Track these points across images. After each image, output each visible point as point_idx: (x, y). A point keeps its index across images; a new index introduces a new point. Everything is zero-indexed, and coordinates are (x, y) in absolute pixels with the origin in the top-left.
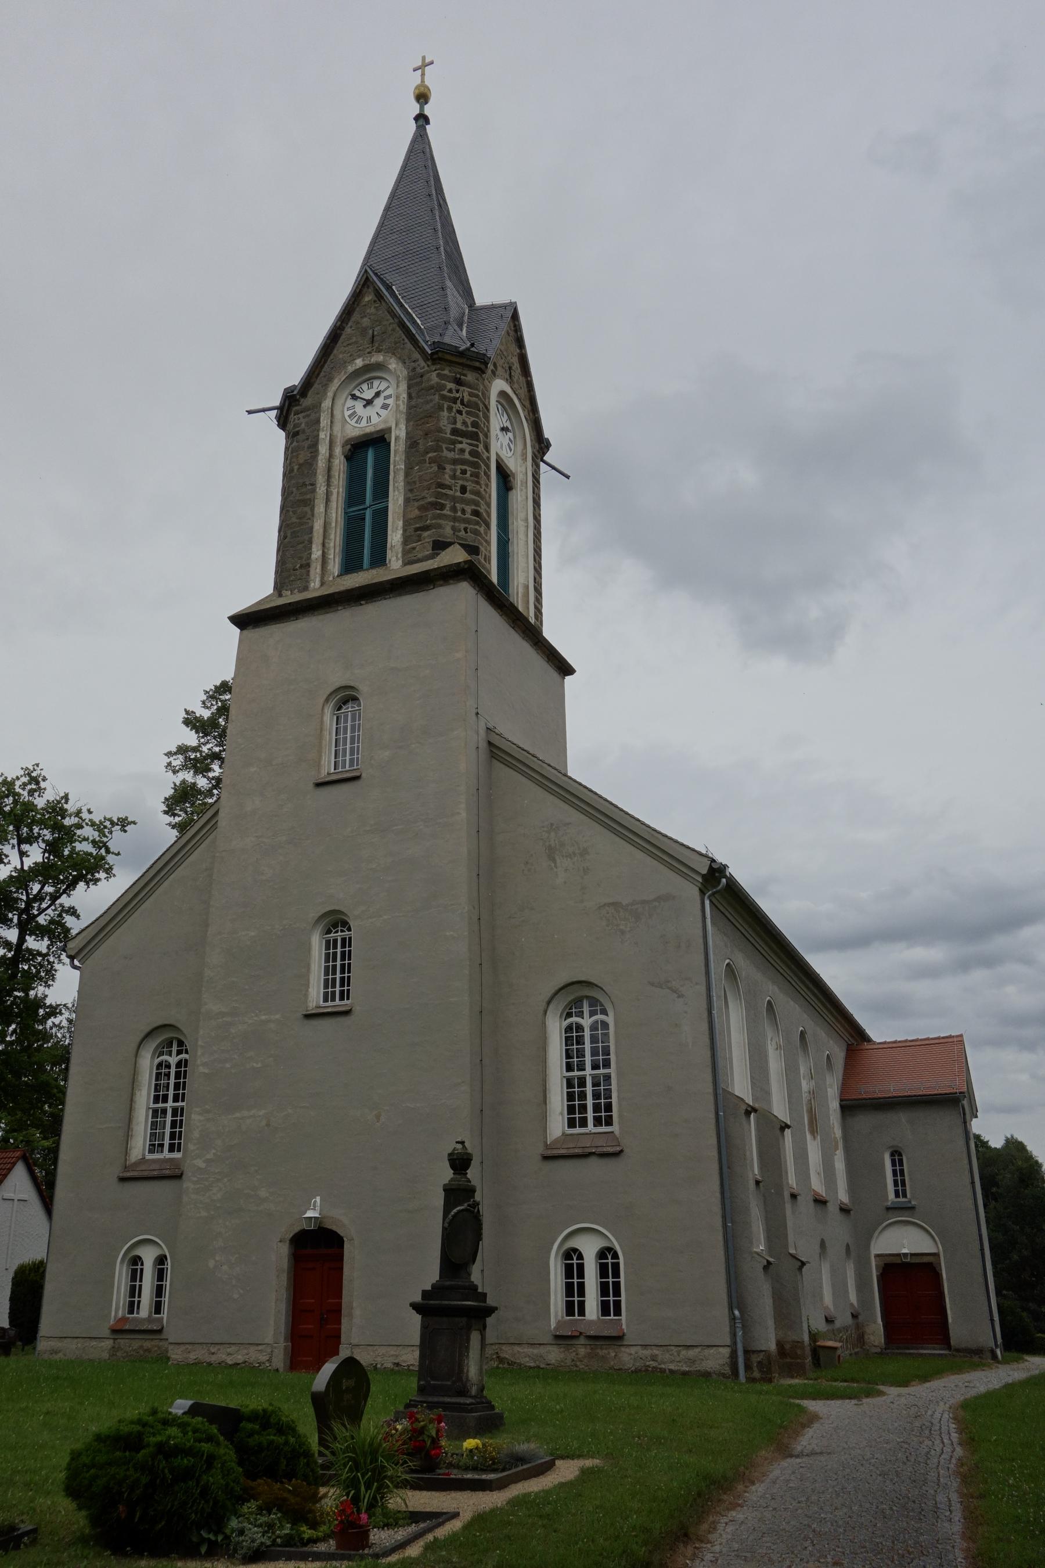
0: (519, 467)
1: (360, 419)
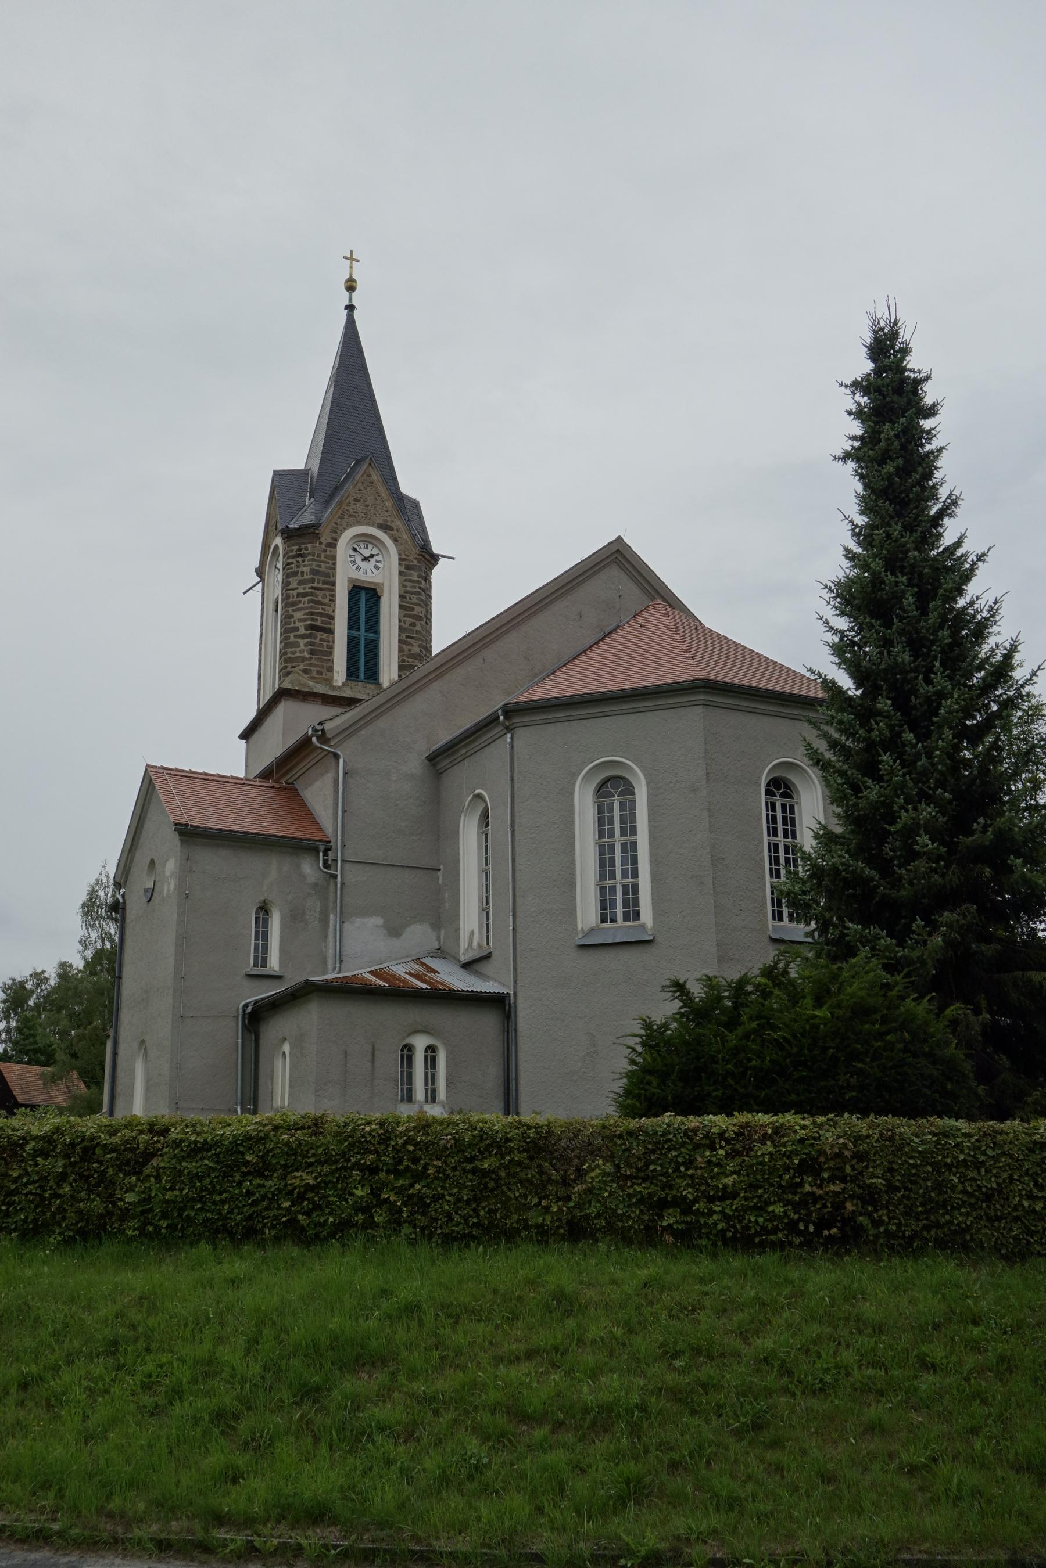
0: (385, 573)
1: (358, 568)
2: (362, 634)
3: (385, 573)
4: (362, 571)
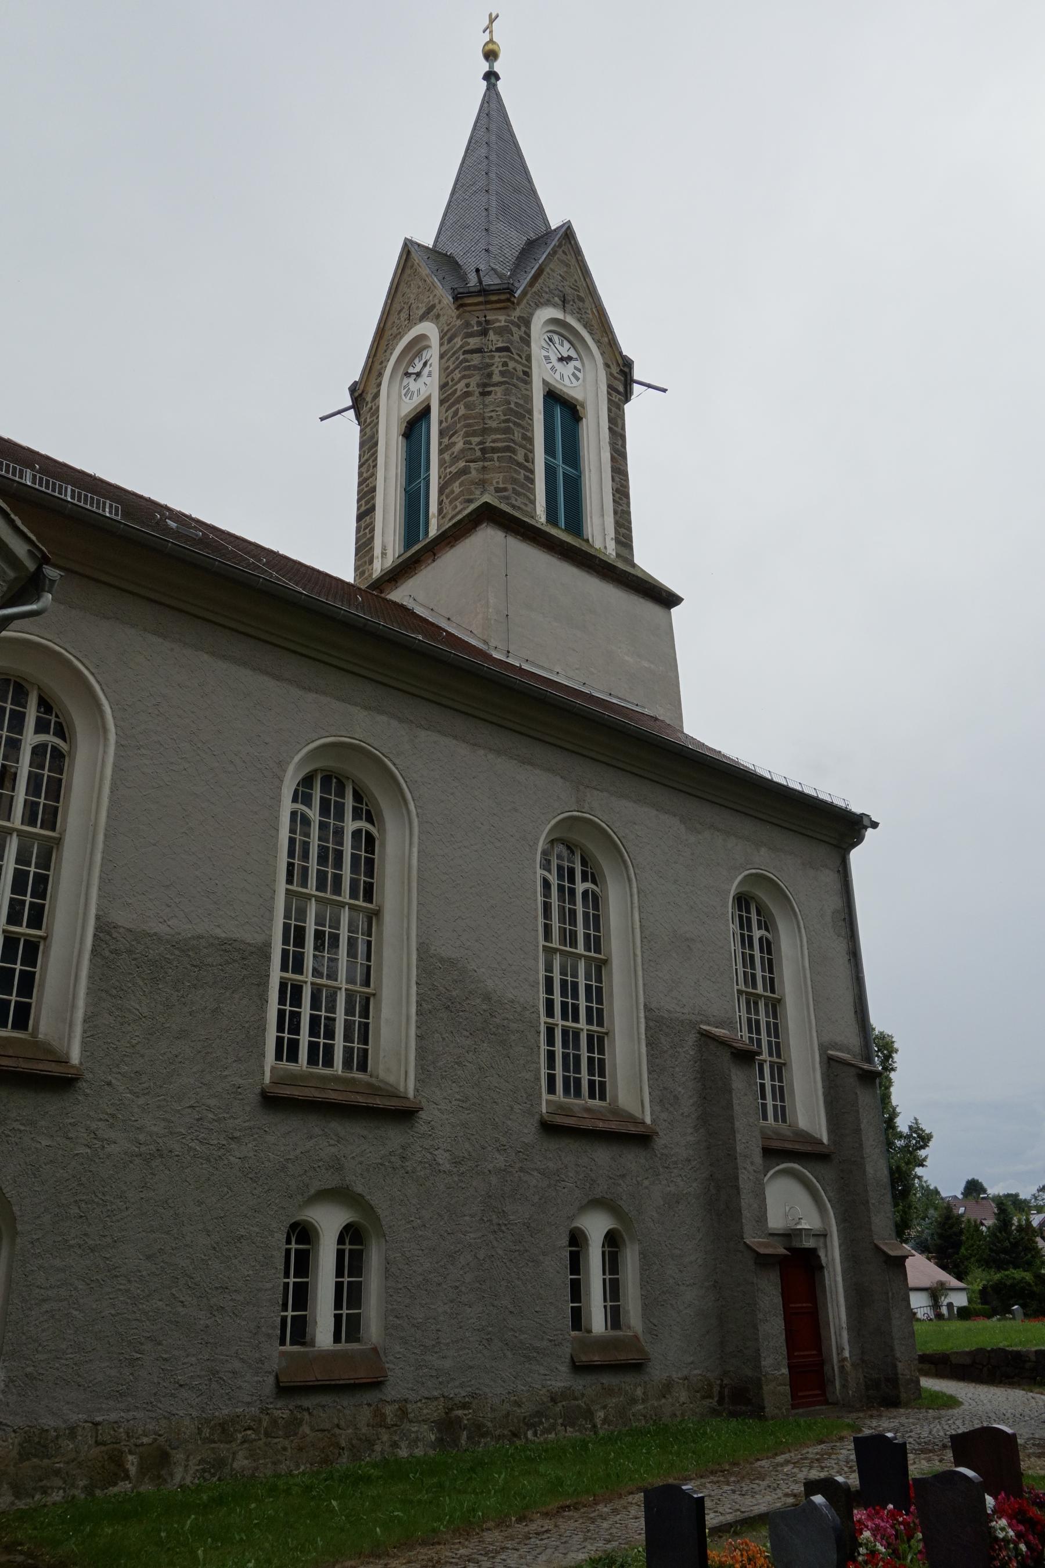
0: (585, 384)
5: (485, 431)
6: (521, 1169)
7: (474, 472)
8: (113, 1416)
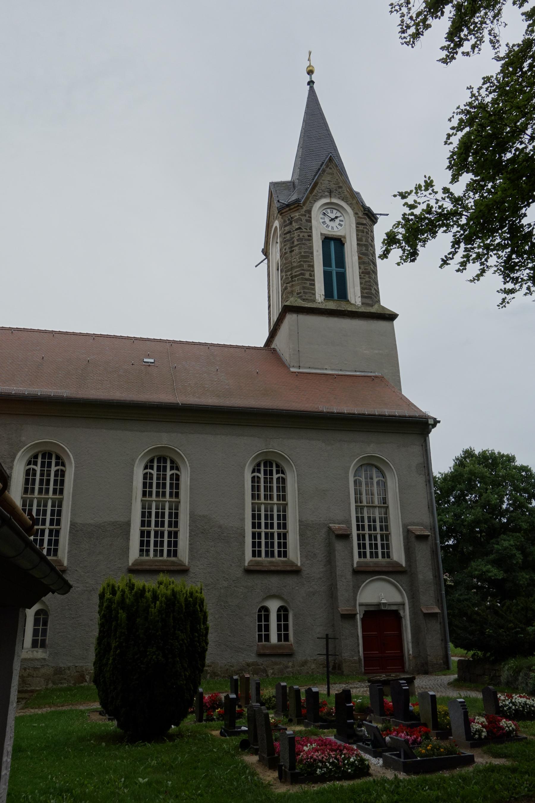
0: (345, 227)
1: (328, 226)
2: (334, 269)
3: (345, 227)
4: (330, 228)
5: (292, 269)
6: (235, 586)
7: (289, 288)
8: (81, 665)
